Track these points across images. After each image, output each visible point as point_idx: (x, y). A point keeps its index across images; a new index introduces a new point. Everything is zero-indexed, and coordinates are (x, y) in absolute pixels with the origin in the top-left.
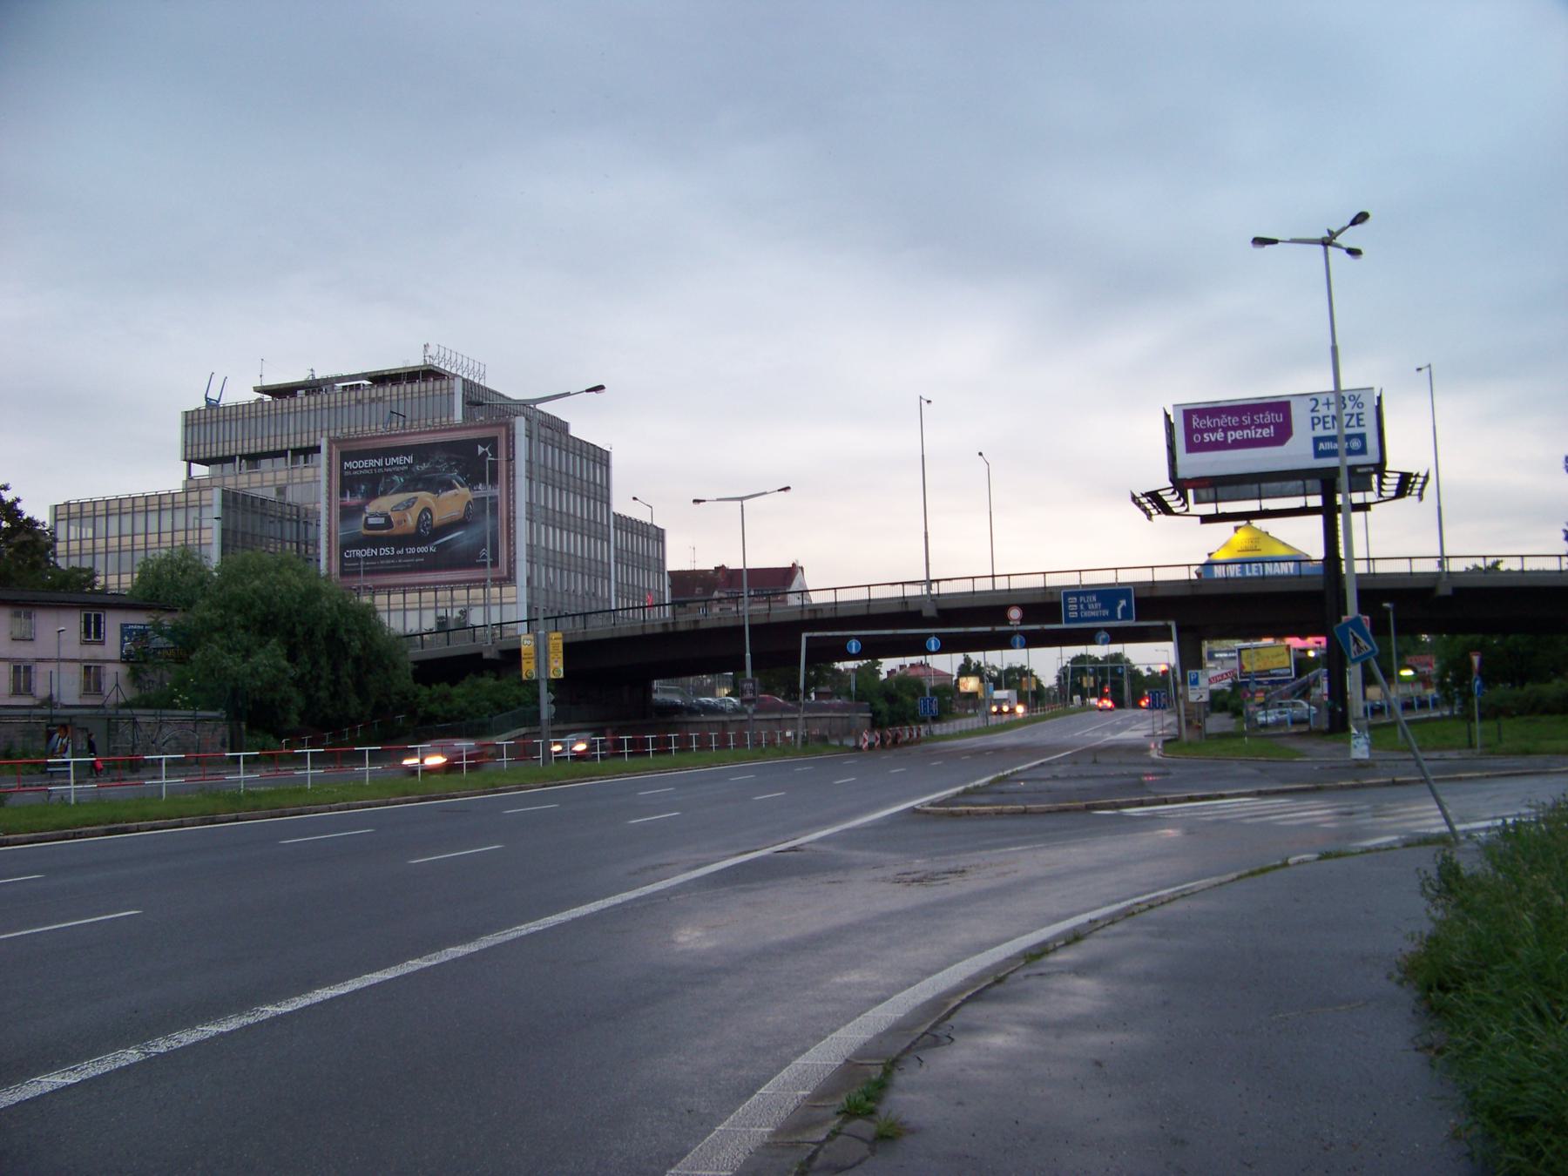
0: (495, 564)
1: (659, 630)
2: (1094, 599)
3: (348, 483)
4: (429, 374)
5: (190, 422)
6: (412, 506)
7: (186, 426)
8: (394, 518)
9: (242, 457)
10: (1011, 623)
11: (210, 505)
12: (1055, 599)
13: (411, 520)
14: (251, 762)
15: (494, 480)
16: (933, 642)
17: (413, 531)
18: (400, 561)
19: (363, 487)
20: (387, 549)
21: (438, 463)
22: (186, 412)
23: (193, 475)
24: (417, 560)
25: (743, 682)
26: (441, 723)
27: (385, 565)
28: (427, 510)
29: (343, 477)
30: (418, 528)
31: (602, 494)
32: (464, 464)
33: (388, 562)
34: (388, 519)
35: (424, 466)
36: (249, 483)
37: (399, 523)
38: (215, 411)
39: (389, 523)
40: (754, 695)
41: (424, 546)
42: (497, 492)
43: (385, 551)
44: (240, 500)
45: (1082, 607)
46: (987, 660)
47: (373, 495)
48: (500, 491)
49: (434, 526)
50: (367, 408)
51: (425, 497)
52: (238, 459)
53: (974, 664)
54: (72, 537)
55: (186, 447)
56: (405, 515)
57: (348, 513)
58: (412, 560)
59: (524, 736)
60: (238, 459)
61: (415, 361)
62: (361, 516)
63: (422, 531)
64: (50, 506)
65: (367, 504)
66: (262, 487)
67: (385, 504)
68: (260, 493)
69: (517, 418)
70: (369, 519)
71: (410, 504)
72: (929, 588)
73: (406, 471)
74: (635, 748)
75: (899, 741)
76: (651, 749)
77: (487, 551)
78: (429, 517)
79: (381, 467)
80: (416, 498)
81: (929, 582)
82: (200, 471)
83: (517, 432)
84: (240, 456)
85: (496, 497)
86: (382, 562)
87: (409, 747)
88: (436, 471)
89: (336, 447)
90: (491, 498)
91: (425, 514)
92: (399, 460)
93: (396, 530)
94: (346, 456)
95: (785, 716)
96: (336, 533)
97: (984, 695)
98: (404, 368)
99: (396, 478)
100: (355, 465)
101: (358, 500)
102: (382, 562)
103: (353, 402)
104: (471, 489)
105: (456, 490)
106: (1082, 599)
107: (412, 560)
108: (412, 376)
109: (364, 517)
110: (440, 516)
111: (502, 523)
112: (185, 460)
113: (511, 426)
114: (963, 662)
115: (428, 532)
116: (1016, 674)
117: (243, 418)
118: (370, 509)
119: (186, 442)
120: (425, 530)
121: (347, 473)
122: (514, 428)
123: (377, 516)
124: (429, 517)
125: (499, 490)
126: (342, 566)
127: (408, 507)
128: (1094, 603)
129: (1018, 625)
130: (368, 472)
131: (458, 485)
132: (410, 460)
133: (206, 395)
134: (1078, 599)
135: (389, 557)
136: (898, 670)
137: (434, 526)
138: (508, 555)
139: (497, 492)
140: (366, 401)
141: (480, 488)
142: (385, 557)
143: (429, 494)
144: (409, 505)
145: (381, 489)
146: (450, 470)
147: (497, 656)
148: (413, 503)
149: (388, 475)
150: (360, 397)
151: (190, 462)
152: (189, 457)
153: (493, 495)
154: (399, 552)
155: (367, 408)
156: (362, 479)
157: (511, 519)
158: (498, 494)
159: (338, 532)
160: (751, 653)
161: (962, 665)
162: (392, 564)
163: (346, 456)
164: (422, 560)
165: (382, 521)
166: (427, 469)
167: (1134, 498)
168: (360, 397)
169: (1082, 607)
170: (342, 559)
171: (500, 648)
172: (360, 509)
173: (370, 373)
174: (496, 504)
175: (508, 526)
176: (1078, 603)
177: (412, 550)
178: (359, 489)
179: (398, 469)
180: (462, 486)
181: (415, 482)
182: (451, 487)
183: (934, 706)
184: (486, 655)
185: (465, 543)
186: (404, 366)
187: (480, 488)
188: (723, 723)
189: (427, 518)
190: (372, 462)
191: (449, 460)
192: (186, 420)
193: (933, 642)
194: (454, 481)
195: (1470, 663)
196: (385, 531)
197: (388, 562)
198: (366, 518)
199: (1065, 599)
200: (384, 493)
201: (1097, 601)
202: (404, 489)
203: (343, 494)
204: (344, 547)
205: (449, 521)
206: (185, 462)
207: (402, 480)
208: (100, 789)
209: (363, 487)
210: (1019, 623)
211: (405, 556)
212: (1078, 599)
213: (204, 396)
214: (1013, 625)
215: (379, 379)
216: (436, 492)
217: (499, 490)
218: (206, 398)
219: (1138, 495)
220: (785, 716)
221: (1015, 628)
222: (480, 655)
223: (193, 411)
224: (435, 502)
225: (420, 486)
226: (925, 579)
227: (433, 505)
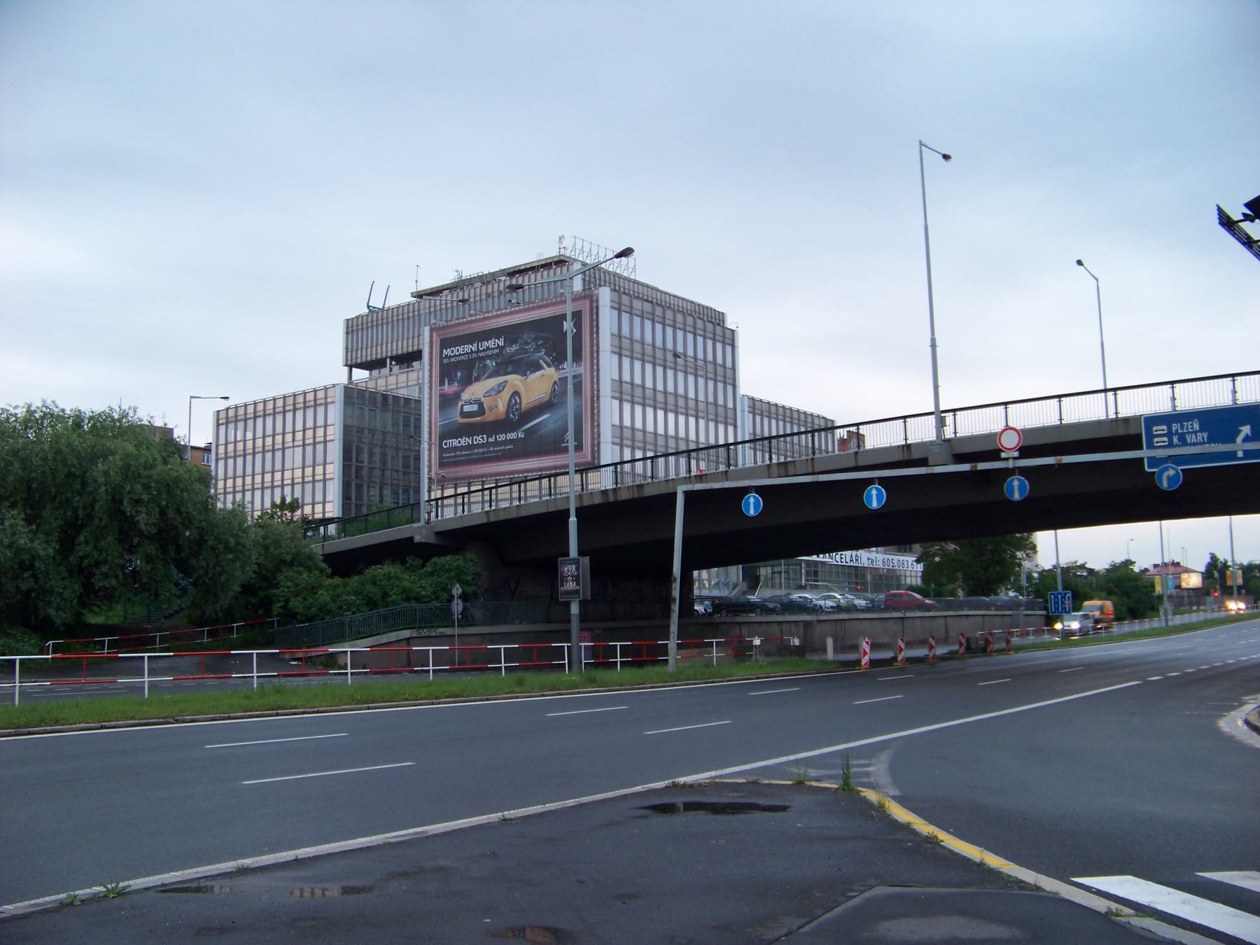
0: (579, 448)
1: (598, 500)
2: (1196, 426)
3: (447, 371)
4: (560, 262)
5: (350, 329)
6: (503, 390)
7: (347, 333)
8: (487, 403)
9: (392, 358)
10: (1003, 455)
11: (333, 402)
12: (1132, 431)
13: (502, 406)
14: (29, 670)
15: (577, 357)
16: (874, 492)
17: (503, 417)
18: (491, 449)
19: (459, 374)
20: (479, 438)
21: (527, 344)
22: (348, 320)
23: (353, 379)
24: (506, 448)
25: (564, 563)
26: (302, 622)
27: (478, 453)
28: (516, 394)
29: (441, 365)
30: (507, 412)
31: (728, 376)
32: (551, 343)
33: (481, 450)
34: (481, 405)
35: (515, 348)
36: (397, 383)
37: (491, 409)
38: (375, 315)
39: (481, 411)
40: (578, 584)
41: (513, 432)
42: (581, 370)
43: (479, 439)
44: (390, 401)
45: (1175, 440)
46: (1235, 559)
47: (468, 381)
48: (584, 369)
49: (522, 411)
50: (496, 300)
51: (514, 380)
52: (388, 360)
53: (1221, 562)
54: (238, 439)
55: (347, 353)
56: (497, 402)
57: (447, 402)
58: (503, 448)
59: (408, 640)
60: (388, 360)
61: (550, 252)
62: (458, 403)
63: (512, 416)
64: (214, 412)
65: (463, 391)
66: (408, 386)
67: (477, 390)
68: (403, 393)
69: (601, 288)
70: (465, 407)
71: (501, 388)
72: (941, 423)
73: (497, 355)
74: (598, 658)
75: (989, 650)
76: (619, 659)
77: (570, 436)
78: (518, 400)
79: (475, 352)
80: (506, 382)
81: (940, 416)
82: (360, 375)
83: (601, 303)
84: (390, 357)
85: (580, 376)
86: (476, 451)
87: (232, 652)
88: (525, 351)
89: (437, 335)
90: (575, 377)
91: (514, 398)
92: (491, 343)
93: (488, 417)
94: (445, 343)
95: (909, 614)
96: (436, 423)
97: (1162, 589)
98: (538, 261)
99: (488, 362)
100: (452, 351)
101: (455, 387)
102: (476, 451)
103: (484, 297)
104: (557, 369)
105: (542, 371)
106: (1175, 427)
107: (503, 448)
108: (547, 265)
109: (460, 404)
110: (528, 400)
111: (586, 406)
112: (346, 365)
113: (594, 298)
114: (1209, 560)
115: (518, 417)
116: (1256, 571)
117: (392, 321)
118: (465, 396)
119: (347, 348)
120: (514, 415)
121: (446, 361)
122: (597, 301)
123: (471, 403)
124: (518, 400)
125: (583, 367)
126: (441, 458)
127: (499, 392)
128: (1195, 432)
129: (1015, 458)
130: (463, 358)
131: (544, 364)
132: (501, 342)
133: (368, 303)
134: (1170, 428)
135: (483, 445)
136: (1151, 569)
137: (522, 411)
138: (593, 438)
139: (581, 370)
140: (496, 294)
141: (565, 367)
142: (479, 446)
143: (519, 377)
144: (499, 389)
145: (475, 374)
146: (538, 349)
147: (432, 540)
148: (504, 387)
149: (483, 359)
150: (490, 290)
151: (351, 367)
152: (349, 362)
153: (577, 373)
154: (491, 440)
155: (496, 300)
156: (458, 365)
157: (595, 398)
158: (582, 371)
159: (438, 422)
160: (577, 517)
161: (1209, 563)
162: (484, 453)
163: (445, 343)
164: (512, 446)
165: (475, 408)
166: (517, 351)
167: (1227, 223)
168: (490, 290)
169: (1175, 440)
170: (442, 450)
171: (435, 530)
172: (457, 396)
173: (509, 269)
174: (581, 382)
175: (592, 408)
176: (1169, 435)
177: (501, 437)
178: (456, 376)
179: (490, 353)
180: (549, 366)
181: (508, 365)
182: (538, 367)
183: (1067, 602)
184: (417, 539)
185: (551, 427)
186: (539, 259)
187: (565, 367)
188: (806, 623)
189: (516, 402)
190: (468, 348)
191: (535, 340)
192: (347, 328)
193: (874, 492)
194: (541, 361)
195: (1235, 702)
196: (478, 419)
197: (481, 450)
198: (462, 406)
199: (1149, 429)
200: (478, 379)
201: (1202, 430)
202: (496, 373)
203: (442, 383)
204: (443, 437)
205: (536, 403)
206: (347, 368)
207: (494, 364)
208: (176, 681)
209: (459, 374)
210: (1016, 454)
211: (496, 443)
212: (1170, 428)
213: (366, 304)
214: (1007, 459)
215: (513, 273)
216: (524, 374)
217: (583, 367)
218: (368, 307)
219: (1236, 213)
220: (909, 614)
221: (1010, 464)
222: (412, 538)
223: (353, 319)
224: (522, 384)
225: (510, 369)
226: (933, 410)
227: (522, 390)
